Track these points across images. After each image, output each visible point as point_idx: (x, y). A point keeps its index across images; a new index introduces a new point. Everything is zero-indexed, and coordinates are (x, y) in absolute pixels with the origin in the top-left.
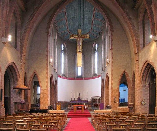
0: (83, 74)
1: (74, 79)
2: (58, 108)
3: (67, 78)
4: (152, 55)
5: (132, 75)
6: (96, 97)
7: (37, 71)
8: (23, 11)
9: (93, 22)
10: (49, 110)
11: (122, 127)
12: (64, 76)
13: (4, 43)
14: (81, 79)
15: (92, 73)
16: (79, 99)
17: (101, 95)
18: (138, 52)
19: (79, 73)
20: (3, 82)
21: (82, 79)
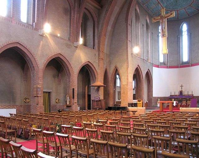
1: (177, 67)
3: (167, 67)
7: (118, 66)
8: (99, 10)
10: (129, 108)
11: (183, 129)
12: (164, 65)
13: (76, 47)
14: (185, 66)
19: (185, 58)
21: (189, 66)
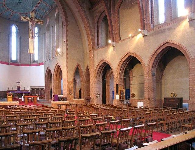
0: (19, 59)
1: (8, 64)
2: (9, 99)
4: (109, 56)
5: (85, 69)
6: (37, 88)
9: (39, 4)
14: (16, 64)
15: (31, 60)
16: (19, 88)
17: (45, 85)
18: (94, 50)
19: (14, 56)
20: (64, 82)
21: (18, 65)
